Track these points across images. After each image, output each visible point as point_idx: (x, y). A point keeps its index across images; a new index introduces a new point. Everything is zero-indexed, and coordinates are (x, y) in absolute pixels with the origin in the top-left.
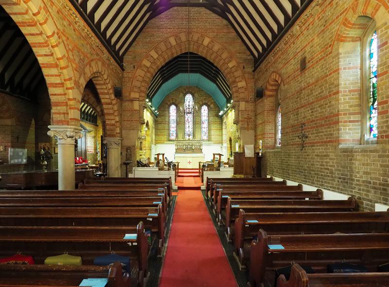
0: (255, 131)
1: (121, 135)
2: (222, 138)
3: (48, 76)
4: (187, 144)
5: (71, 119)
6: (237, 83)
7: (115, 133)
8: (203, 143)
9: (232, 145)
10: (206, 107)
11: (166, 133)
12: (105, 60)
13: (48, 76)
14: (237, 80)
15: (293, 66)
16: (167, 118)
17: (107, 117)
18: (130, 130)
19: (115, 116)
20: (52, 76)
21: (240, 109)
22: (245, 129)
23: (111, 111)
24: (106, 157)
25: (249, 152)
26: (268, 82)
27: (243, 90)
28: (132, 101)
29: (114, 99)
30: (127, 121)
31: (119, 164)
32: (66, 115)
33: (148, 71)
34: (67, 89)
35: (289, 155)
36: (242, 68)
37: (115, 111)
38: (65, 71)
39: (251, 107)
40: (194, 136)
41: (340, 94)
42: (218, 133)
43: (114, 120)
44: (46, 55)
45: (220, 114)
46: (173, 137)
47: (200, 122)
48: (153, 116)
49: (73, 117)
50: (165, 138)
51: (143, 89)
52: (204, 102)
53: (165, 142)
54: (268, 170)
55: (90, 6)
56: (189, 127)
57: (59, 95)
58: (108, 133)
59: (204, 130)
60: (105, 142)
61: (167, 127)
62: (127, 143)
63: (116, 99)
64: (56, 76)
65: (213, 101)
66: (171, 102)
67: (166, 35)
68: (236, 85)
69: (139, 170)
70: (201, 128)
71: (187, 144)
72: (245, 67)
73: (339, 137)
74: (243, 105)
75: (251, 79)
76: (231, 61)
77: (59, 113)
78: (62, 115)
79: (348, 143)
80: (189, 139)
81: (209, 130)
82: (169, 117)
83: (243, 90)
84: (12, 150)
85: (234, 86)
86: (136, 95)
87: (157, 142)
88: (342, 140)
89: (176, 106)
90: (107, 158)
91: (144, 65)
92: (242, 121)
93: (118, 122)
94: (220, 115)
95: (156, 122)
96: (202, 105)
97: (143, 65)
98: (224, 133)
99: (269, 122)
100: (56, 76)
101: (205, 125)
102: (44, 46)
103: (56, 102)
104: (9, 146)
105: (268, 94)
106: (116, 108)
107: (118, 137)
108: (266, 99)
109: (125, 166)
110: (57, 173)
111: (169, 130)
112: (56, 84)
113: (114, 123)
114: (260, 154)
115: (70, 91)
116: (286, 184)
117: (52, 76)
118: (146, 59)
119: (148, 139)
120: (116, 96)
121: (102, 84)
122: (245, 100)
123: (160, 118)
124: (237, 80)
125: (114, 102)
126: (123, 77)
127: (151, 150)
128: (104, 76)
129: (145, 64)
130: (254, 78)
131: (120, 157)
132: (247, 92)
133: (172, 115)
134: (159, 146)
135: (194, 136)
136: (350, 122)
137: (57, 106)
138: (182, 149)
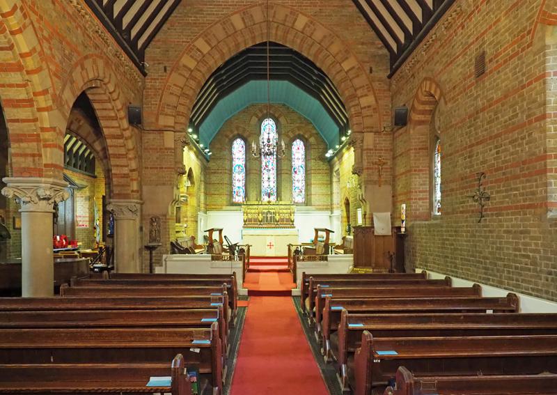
0: (394, 187)
1: (141, 195)
2: (332, 200)
5: (46, 165)
6: (359, 98)
7: (129, 192)
10: (302, 143)
11: (225, 190)
12: (110, 56)
14: (359, 93)
17: (113, 161)
19: (130, 159)
20: (11, 86)
21: (365, 147)
22: (375, 183)
24: (111, 236)
26: (416, 96)
29: (128, 129)
30: (151, 168)
31: (138, 248)
32: (37, 158)
34: (40, 110)
36: (368, 71)
37: (129, 150)
38: (35, 78)
39: (384, 142)
41: (548, 120)
42: (324, 190)
46: (239, 199)
47: (291, 171)
48: (200, 160)
49: (49, 162)
50: (224, 199)
52: (297, 133)
53: (224, 208)
55: (117, 9)
56: (269, 179)
58: (116, 190)
60: (109, 208)
61: (226, 180)
62: (151, 210)
64: (18, 86)
65: (314, 132)
66: (236, 132)
67: (225, 11)
69: (175, 259)
70: (291, 181)
71: (265, 211)
74: (369, 139)
76: (347, 58)
77: (25, 155)
78: (30, 159)
81: (308, 184)
82: (231, 160)
85: (353, 103)
86: (170, 121)
87: (208, 208)
90: (113, 237)
92: (367, 168)
93: (134, 170)
94: (327, 158)
95: (205, 170)
97: (181, 64)
100: (18, 86)
101: (299, 177)
105: (417, 119)
106: (130, 144)
107: (133, 198)
108: (414, 129)
110: (21, 264)
111: (231, 184)
114: (403, 230)
116: (450, 285)
117: (11, 86)
119: (192, 201)
120: (131, 122)
123: (215, 166)
126: (144, 88)
127: (197, 222)
128: (109, 85)
130: (389, 90)
134: (210, 213)
135: (279, 196)
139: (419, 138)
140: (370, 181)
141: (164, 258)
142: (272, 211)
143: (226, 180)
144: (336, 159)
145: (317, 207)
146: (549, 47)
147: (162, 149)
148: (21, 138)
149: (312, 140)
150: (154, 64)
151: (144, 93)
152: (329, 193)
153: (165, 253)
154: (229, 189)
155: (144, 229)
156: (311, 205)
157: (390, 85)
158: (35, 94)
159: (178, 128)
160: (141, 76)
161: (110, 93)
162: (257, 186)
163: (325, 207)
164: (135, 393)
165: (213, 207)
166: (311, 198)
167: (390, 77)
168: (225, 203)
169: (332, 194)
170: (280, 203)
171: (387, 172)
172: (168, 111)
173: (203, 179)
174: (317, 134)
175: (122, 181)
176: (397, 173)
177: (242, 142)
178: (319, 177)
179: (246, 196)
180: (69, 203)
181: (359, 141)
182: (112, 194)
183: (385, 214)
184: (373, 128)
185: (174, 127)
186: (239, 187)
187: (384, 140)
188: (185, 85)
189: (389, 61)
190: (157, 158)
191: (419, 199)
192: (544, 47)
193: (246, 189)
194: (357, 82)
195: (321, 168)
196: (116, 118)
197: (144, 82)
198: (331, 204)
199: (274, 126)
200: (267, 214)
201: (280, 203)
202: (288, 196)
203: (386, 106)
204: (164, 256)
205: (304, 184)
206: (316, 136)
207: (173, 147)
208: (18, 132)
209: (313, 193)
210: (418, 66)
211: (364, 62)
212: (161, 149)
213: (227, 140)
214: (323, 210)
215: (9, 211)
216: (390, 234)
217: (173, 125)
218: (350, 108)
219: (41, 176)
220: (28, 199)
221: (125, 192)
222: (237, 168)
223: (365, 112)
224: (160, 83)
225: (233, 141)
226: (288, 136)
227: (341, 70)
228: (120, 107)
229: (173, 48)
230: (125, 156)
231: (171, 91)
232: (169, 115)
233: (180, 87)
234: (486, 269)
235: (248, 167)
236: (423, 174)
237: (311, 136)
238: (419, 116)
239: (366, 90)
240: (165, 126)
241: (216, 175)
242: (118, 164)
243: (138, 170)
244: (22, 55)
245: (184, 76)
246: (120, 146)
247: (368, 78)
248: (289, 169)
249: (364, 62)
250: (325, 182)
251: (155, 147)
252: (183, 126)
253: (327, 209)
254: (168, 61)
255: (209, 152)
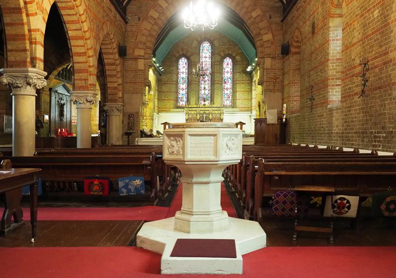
0: (283, 93)
1: (123, 100)
2: (251, 104)
3: (74, 46)
4: (202, 112)
5: (90, 85)
6: (262, 35)
7: (117, 98)
8: (225, 110)
9: (261, 112)
10: (231, 60)
11: (173, 97)
12: (112, 18)
13: (74, 46)
14: (262, 32)
15: (307, 29)
16: (175, 76)
17: (109, 79)
18: (133, 93)
19: (118, 78)
20: (78, 46)
21: (265, 68)
22: (271, 91)
23: (114, 73)
25: (272, 118)
26: (293, 37)
27: (269, 45)
28: (136, 59)
29: (118, 59)
30: (129, 83)
31: (121, 134)
32: (87, 81)
33: (156, 24)
34: (89, 57)
35: (304, 118)
36: (268, 18)
37: (118, 72)
38: (88, 42)
39: (277, 64)
40: (212, 101)
41: (329, 62)
42: (246, 96)
43: (116, 82)
44: (76, 30)
45: (249, 69)
46: (182, 103)
47: (222, 81)
48: (156, 74)
49: (92, 83)
50: (171, 103)
51: (149, 44)
52: (227, 53)
53: (172, 110)
54: (291, 137)
56: (205, 87)
57: (82, 63)
58: (109, 97)
59: (226, 92)
60: (106, 108)
61: (174, 89)
62: (129, 109)
63: (119, 58)
64: (81, 46)
65: (240, 51)
66: (181, 53)
68: (261, 38)
69: (143, 140)
70: (222, 89)
71: (202, 112)
72: (272, 16)
73: (327, 99)
74: (268, 62)
75: (279, 30)
76: (255, 9)
77: (81, 80)
78: (84, 82)
79: (335, 103)
80: (204, 105)
81: (234, 92)
82: (178, 74)
83: (269, 45)
84: (7, 117)
85: (259, 39)
86: (142, 52)
87: (160, 110)
88: (330, 101)
89: (188, 58)
90: (106, 127)
91: (151, 17)
92: (267, 82)
93: (120, 85)
94: (248, 72)
95: (159, 81)
96: (225, 57)
97: (149, 16)
98: (253, 96)
99: (295, 83)
100: (81, 46)
101: (228, 85)
102: (76, 23)
103: (78, 70)
104: (3, 113)
105: (294, 51)
106: (119, 68)
107: (120, 102)
108: (292, 57)
109: (127, 137)
111: (177, 92)
112: (80, 53)
113: (116, 86)
114: (284, 120)
115: (91, 59)
117: (78, 46)
118: (153, 9)
119: (151, 105)
120: (120, 55)
121: (108, 44)
122: (271, 56)
123: (166, 79)
124: (262, 32)
125: (118, 62)
126: (126, 31)
127: (153, 120)
129: (152, 15)
130: (282, 30)
131: (121, 126)
132: (274, 46)
133: (181, 71)
134: (162, 114)
135: (212, 101)
136: (337, 85)
137: (80, 73)
138: (194, 120)
139: (295, 63)
140: (268, 89)
141: (136, 141)
142: (207, 112)
143: (174, 89)
144: (254, 72)
145: (241, 109)
146: (331, 27)
147: (137, 71)
148: (80, 71)
149: (238, 58)
150: (133, 15)
151: (126, 34)
152: (250, 98)
153: (136, 137)
154: (175, 96)
155: (124, 122)
156: (236, 108)
157: (283, 27)
158: (88, 49)
159: (146, 56)
160: (125, 24)
161: (111, 39)
162: (196, 93)
163: (247, 109)
164: (188, 89)
165: (163, 109)
166: (236, 102)
167: (282, 21)
168: (172, 106)
169: (251, 98)
170: (213, 106)
171: (279, 83)
172: (141, 46)
173: (157, 89)
174: (241, 53)
175: (113, 91)
176: (285, 85)
177: (186, 60)
178: (242, 86)
179: (188, 101)
180: (69, 106)
181: (262, 64)
182: (106, 100)
183: (274, 110)
184: (270, 55)
185: (144, 56)
186: (183, 94)
187: (278, 63)
188: (151, 29)
189: (282, 10)
190: (133, 77)
191: (295, 101)
192: (329, 27)
193: (188, 95)
194: (261, 25)
195: (244, 79)
196: (111, 54)
197: (126, 28)
198: (251, 107)
199: (210, 47)
200: (203, 114)
201: (213, 106)
202: (219, 100)
203: (280, 40)
204: (137, 139)
205: (231, 91)
206: (241, 54)
207: (143, 69)
208: (79, 68)
209: (237, 98)
210: (294, 18)
211: (266, 12)
212: (135, 70)
213: (175, 59)
214: (245, 111)
215: (41, 112)
216: (277, 123)
217: (143, 55)
218: (257, 41)
219: (88, 90)
220: (82, 102)
221: (115, 98)
222: (181, 80)
223: (266, 45)
224: (136, 28)
225: (179, 59)
226: (220, 55)
227: (251, 17)
228: (86, 29)
229: (144, 5)
230: (115, 76)
231: (142, 33)
232: (141, 49)
233: (148, 30)
234: (313, 136)
235: (190, 79)
236: (297, 85)
237: (237, 55)
238: (296, 49)
239: (267, 30)
240: (139, 56)
241: (166, 85)
242: (111, 81)
243: (122, 84)
244: (84, 32)
245: (151, 23)
246: (114, 70)
247: (268, 22)
248: (220, 80)
249: (266, 12)
250: (247, 90)
251: (132, 69)
252: (149, 56)
253: (248, 110)
254: (141, 13)
255: (162, 69)
